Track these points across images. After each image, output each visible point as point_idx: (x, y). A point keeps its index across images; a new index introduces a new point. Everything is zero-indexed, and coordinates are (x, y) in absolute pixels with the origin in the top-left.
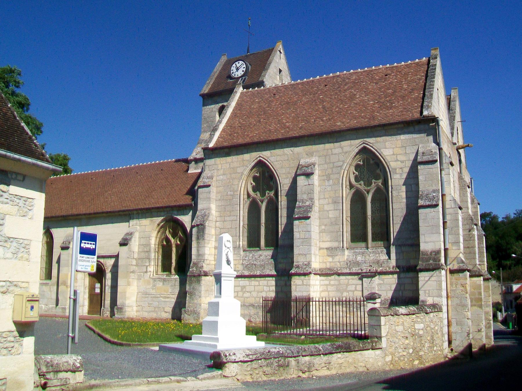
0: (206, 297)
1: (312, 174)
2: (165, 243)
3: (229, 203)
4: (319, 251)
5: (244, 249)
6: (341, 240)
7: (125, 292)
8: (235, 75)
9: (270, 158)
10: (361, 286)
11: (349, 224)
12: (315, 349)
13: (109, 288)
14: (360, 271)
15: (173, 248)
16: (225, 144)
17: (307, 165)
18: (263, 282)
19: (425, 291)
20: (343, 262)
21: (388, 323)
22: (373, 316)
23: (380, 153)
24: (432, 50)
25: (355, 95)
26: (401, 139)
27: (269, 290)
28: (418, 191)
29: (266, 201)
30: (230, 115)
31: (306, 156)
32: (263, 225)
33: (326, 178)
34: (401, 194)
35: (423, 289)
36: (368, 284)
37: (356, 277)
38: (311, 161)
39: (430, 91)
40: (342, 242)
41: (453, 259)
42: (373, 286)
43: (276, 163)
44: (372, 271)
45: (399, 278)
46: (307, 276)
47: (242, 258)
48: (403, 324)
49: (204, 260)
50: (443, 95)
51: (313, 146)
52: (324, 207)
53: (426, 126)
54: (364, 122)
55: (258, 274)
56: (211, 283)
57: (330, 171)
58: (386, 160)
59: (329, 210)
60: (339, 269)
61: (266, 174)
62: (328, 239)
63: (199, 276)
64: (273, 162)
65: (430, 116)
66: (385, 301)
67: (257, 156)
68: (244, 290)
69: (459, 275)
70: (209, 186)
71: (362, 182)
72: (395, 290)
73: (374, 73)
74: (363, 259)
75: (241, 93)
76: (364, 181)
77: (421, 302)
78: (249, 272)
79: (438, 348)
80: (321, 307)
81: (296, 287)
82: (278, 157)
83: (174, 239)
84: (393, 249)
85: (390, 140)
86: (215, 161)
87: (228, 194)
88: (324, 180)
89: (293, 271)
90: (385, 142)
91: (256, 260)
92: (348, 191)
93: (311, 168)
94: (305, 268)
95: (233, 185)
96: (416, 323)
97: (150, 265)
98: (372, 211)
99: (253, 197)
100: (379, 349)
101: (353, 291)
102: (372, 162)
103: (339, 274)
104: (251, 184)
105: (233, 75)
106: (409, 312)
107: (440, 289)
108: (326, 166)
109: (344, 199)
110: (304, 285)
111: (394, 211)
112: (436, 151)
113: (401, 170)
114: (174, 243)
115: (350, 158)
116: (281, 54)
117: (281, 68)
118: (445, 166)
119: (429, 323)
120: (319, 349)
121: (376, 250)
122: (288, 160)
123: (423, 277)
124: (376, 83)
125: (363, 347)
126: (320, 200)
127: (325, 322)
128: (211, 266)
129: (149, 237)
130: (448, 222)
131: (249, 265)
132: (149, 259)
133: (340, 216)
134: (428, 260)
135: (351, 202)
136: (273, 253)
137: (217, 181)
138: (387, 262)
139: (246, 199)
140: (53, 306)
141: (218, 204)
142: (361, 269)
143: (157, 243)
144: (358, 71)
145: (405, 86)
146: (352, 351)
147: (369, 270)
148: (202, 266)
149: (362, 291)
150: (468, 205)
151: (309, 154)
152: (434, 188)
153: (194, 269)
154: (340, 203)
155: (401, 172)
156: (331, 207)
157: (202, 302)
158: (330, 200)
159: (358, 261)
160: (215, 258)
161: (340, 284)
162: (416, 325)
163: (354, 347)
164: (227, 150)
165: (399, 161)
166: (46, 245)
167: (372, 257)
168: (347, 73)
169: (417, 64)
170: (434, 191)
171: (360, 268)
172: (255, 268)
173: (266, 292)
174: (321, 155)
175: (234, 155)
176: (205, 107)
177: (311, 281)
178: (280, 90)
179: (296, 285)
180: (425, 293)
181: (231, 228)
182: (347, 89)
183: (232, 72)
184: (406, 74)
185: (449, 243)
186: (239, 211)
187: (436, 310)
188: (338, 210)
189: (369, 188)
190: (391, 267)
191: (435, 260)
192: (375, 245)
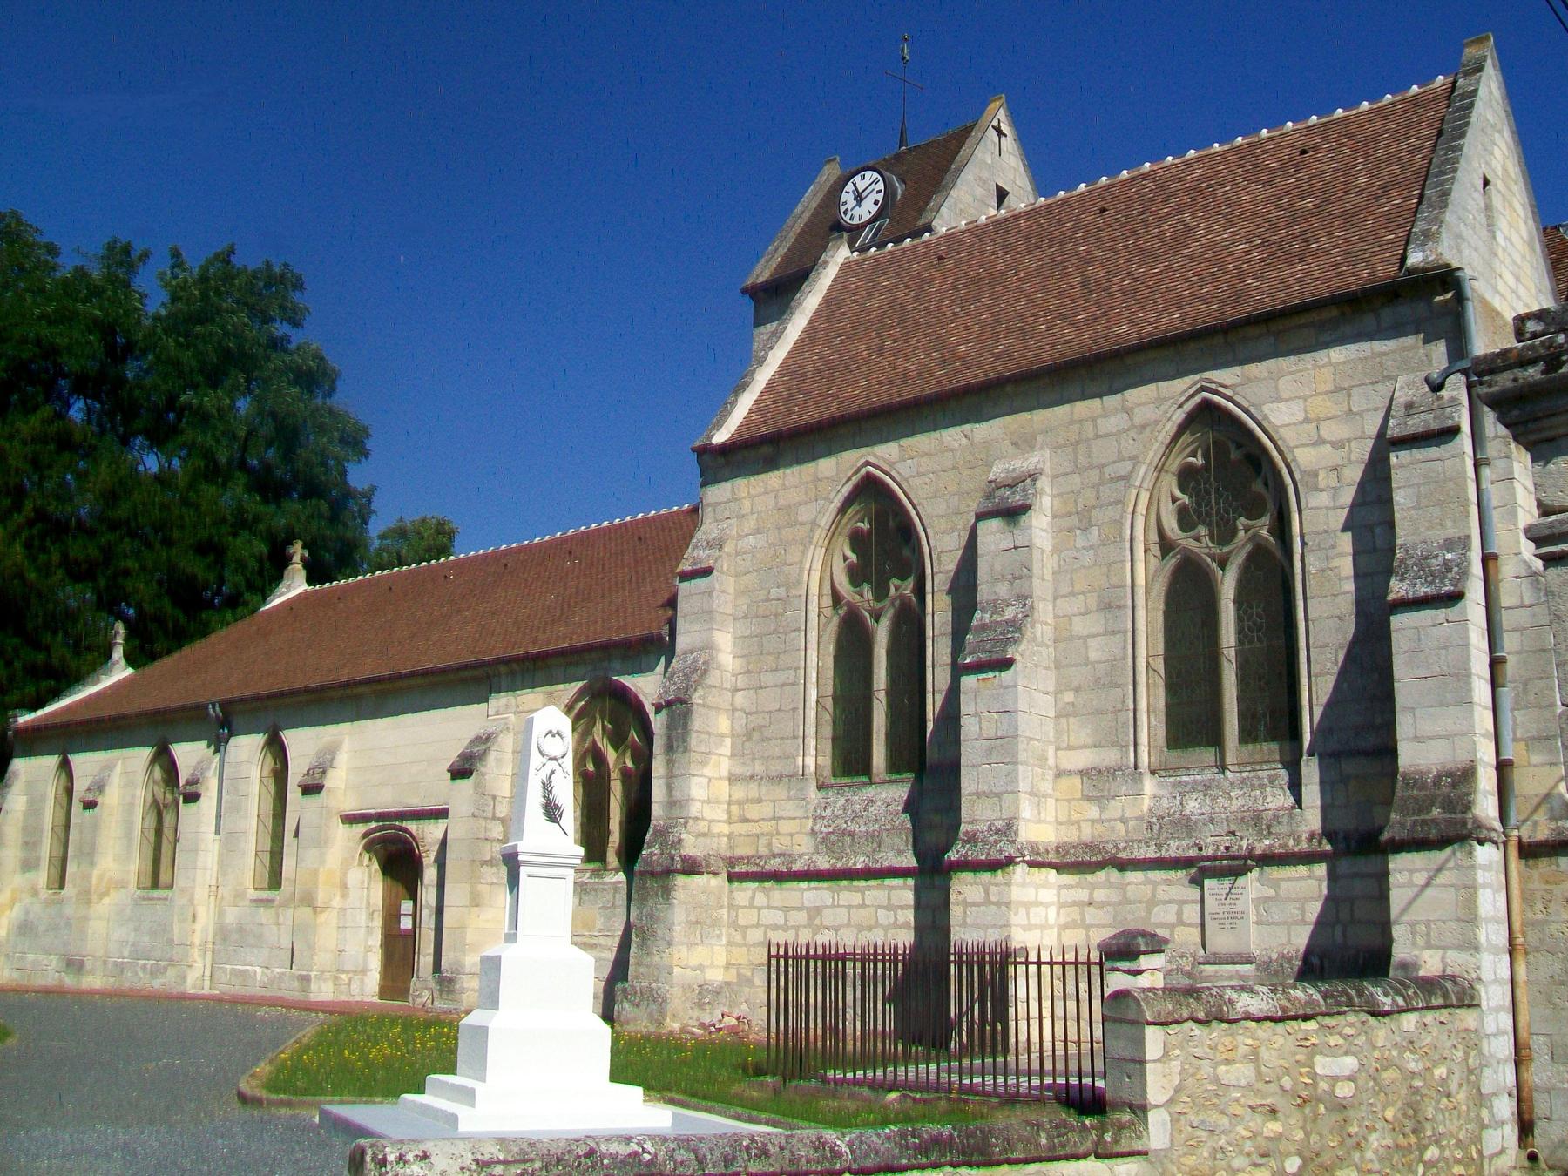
0: (690, 945)
1: (1025, 508)
2: (591, 767)
3: (773, 627)
4: (1055, 783)
6: (1128, 742)
7: (463, 928)
8: (851, 218)
9: (897, 466)
10: (1198, 907)
11: (1161, 683)
12: (816, 1149)
13: (430, 916)
14: (1192, 853)
15: (612, 783)
16: (764, 430)
17: (1010, 482)
18: (874, 892)
19: (1413, 924)
20: (1137, 819)
21: (1177, 1052)
22: (1121, 1021)
23: (1260, 418)
24: (1468, 45)
25: (1191, 229)
26: (1333, 361)
27: (895, 923)
28: (1393, 550)
29: (890, 613)
30: (797, 338)
31: (1012, 450)
32: (882, 695)
33: (1077, 524)
34: (1335, 563)
35: (1406, 918)
36: (1223, 901)
37: (1181, 874)
38: (1025, 464)
39: (1442, 183)
40: (1132, 749)
41: (1535, 801)
42: (1240, 906)
43: (918, 481)
44: (1234, 851)
45: (1332, 876)
46: (999, 872)
47: (811, 811)
48: (1254, 1056)
50: (1518, 207)
51: (1035, 412)
52: (1071, 625)
53: (1421, 308)
54: (1204, 313)
55: (859, 866)
56: (713, 898)
57: (1088, 496)
58: (1279, 443)
59: (1088, 636)
60: (1122, 845)
61: (891, 524)
63: (668, 872)
65: (1433, 269)
66: (1282, 965)
67: (858, 460)
68: (817, 922)
69: (1558, 866)
70: (707, 572)
71: (1203, 531)
72: (1321, 924)
73: (1265, 152)
75: (843, 266)
76: (1209, 525)
77: (1396, 969)
78: (833, 861)
79: (1447, 1153)
80: (1058, 984)
81: (965, 912)
82: (924, 459)
83: (616, 749)
84: (1311, 771)
85: (1295, 368)
86: (733, 487)
88: (1071, 530)
89: (953, 855)
90: (1275, 377)
91: (855, 816)
92: (1154, 562)
93: (1024, 490)
94: (996, 843)
95: (785, 564)
96: (1321, 1053)
98: (1240, 632)
99: (849, 603)
100: (1139, 1153)
102: (1235, 454)
103: (1123, 866)
104: (845, 558)
105: (847, 219)
106: (1283, 1009)
107: (1470, 917)
108: (1076, 479)
109: (1140, 592)
110: (993, 903)
111: (1311, 627)
113: (1333, 475)
114: (615, 765)
115: (1157, 445)
116: (1003, 138)
117: (1005, 184)
119: (1395, 1053)
120: (832, 1150)
121: (1253, 774)
122: (954, 468)
123: (1406, 870)
124: (1267, 183)
125: (1052, 1147)
126: (1059, 601)
127: (1076, 1038)
128: (715, 840)
130: (1512, 662)
134: (1423, 807)
135: (1167, 604)
136: (911, 794)
137: (737, 554)
138: (1291, 816)
139: (829, 612)
140: (284, 970)
142: (1196, 845)
144: (1212, 151)
145: (1361, 181)
146: (999, 1163)
147: (1227, 848)
148: (680, 841)
149: (1203, 925)
152: (1452, 532)
153: (656, 850)
154: (1125, 606)
155: (1333, 482)
157: (675, 961)
158: (1092, 601)
159: (1188, 818)
160: (729, 812)
161: (1125, 901)
162: (1318, 1059)
163: (1009, 1144)
164: (766, 450)
166: (271, 781)
167: (1238, 801)
168: (1176, 161)
169: (1415, 101)
170: (1449, 545)
172: (850, 846)
173: (886, 929)
174: (1061, 441)
175: (790, 465)
176: (762, 329)
177: (1014, 888)
178: (962, 243)
179: (966, 904)
180: (1413, 933)
182: (1167, 214)
183: (842, 209)
184: (1373, 140)
187: (1439, 1001)
188: (1119, 632)
189: (1225, 549)
190: (1305, 836)
191: (1449, 805)
192: (1251, 755)
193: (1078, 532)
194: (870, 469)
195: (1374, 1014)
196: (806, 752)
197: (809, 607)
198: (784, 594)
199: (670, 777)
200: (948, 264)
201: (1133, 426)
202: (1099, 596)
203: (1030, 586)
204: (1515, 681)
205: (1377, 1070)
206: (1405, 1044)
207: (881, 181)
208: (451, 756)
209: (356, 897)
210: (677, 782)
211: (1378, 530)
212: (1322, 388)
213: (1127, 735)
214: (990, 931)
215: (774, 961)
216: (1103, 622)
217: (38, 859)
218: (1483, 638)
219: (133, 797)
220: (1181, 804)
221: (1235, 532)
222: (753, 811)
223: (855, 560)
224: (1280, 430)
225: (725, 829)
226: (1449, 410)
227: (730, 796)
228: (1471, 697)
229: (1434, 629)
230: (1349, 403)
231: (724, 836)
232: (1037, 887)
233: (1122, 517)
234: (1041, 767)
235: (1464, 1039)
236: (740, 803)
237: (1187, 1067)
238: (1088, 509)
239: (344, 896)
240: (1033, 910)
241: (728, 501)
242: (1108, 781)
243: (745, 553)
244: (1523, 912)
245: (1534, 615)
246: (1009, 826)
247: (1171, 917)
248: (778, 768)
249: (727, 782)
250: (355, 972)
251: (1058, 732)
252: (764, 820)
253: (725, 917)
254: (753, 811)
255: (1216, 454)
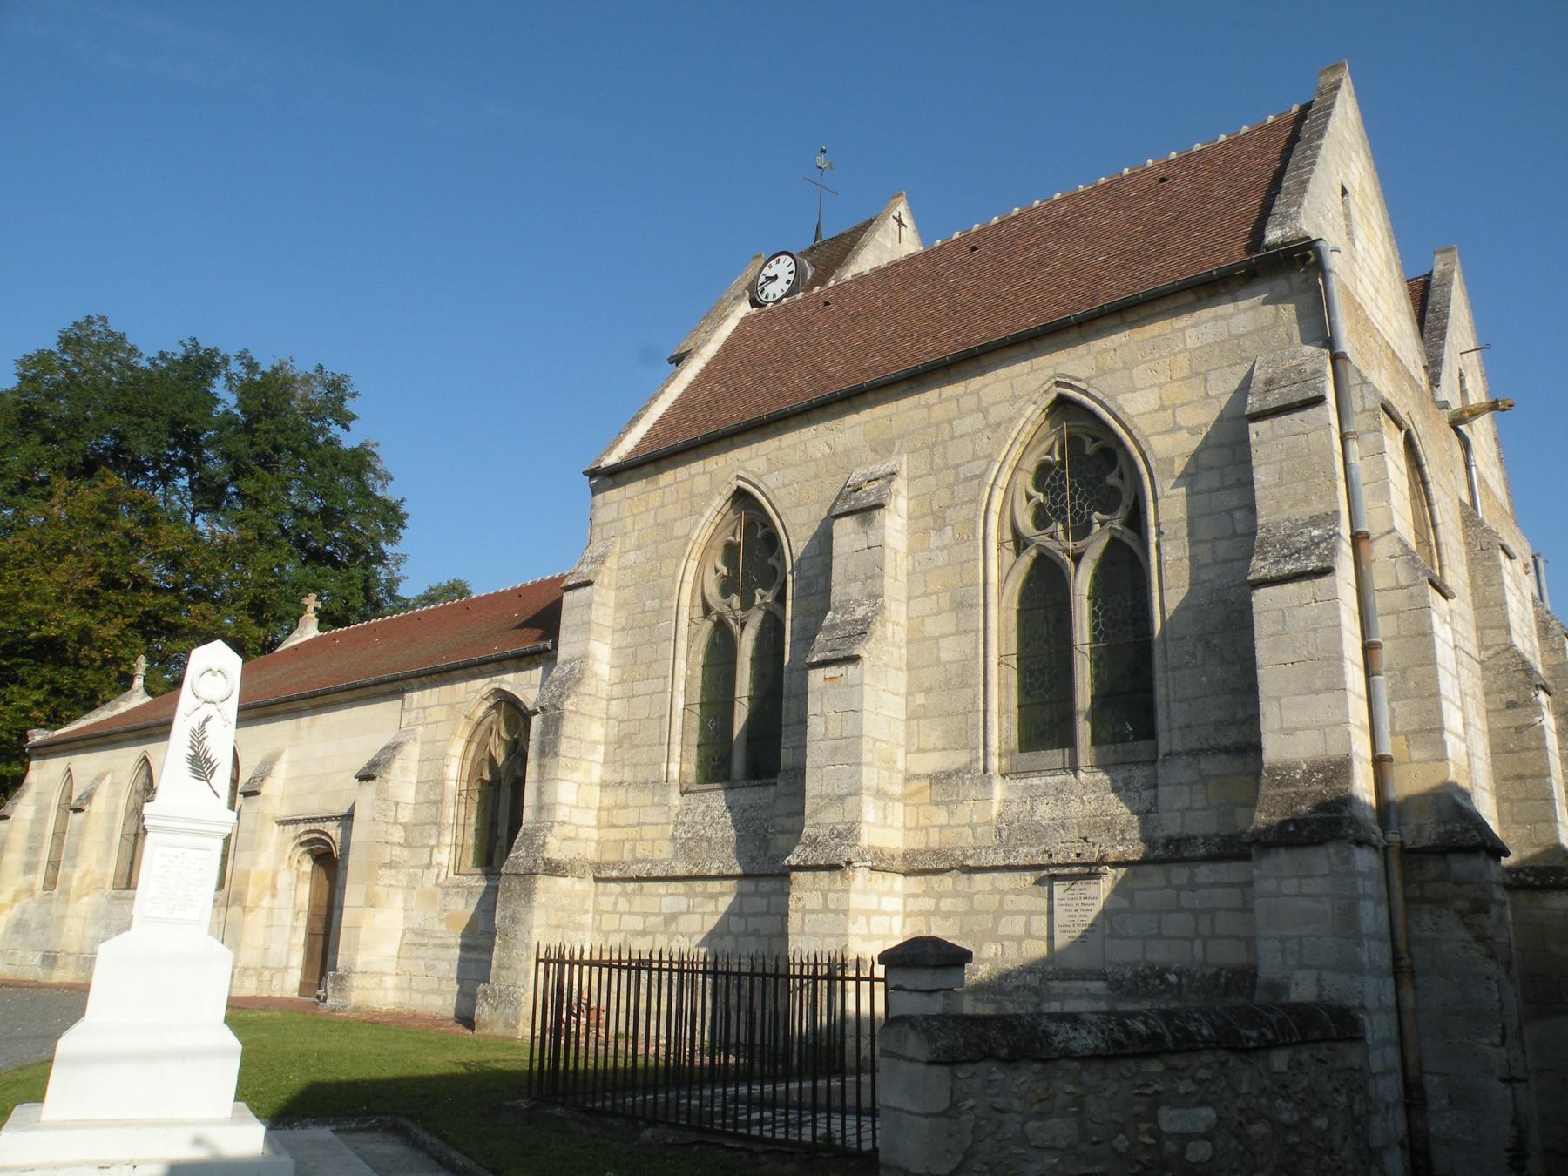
3: (646, 638)
5: (685, 786)
9: (764, 479)
10: (1044, 918)
14: (1042, 859)
20: (985, 824)
22: (899, 1057)
23: (1114, 409)
26: (1189, 347)
31: (870, 456)
33: (932, 524)
38: (882, 469)
43: (783, 492)
44: (1086, 858)
45: (740, 895)
47: (673, 817)
49: (552, 822)
59: (941, 637)
60: (971, 852)
62: (934, 737)
64: (773, 491)
68: (673, 928)
70: (589, 583)
74: (1058, 813)
76: (1064, 521)
87: (646, 609)
89: (792, 860)
92: (1009, 556)
94: (837, 846)
97: (438, 845)
101: (1019, 940)
102: (1090, 448)
104: (717, 571)
105: (763, 297)
106: (1118, 1044)
108: (932, 480)
112: (1317, 366)
118: (1357, 423)
119: (1263, 1101)
122: (817, 477)
129: (442, 758)
130: (1387, 647)
131: (691, 843)
132: (438, 824)
133: (977, 654)
141: (617, 645)
142: (1046, 852)
143: (466, 777)
150: (1505, 616)
151: (879, 449)
152: (1318, 507)
156: (947, 623)
158: (945, 601)
160: (599, 819)
161: (972, 911)
162: (1164, 1113)
165: (1180, 428)
170: (1315, 521)
171: (1043, 847)
172: (708, 852)
173: (736, 937)
179: (804, 911)
181: (648, 718)
185: (1393, 733)
186: (671, 661)
187: (1317, 1034)
188: (971, 631)
193: (933, 532)
194: (741, 483)
195: (1233, 1050)
196: (671, 758)
197: (680, 618)
198: (658, 606)
199: (541, 780)
200: (833, 307)
201: (988, 425)
202: (951, 596)
203: (882, 586)
204: (1391, 670)
205: (1240, 1124)
206: (1275, 1088)
207: (793, 264)
208: (361, 763)
209: (284, 898)
210: (548, 787)
211: (1237, 515)
212: (1178, 374)
213: (977, 737)
214: (828, 940)
215: (542, 965)
216: (955, 621)
217: (38, 862)
218: (1355, 621)
219: (117, 806)
220: (1032, 809)
221: (1089, 525)
222: (621, 817)
223: (725, 572)
224: (1135, 419)
225: (594, 834)
226: (1312, 382)
227: (601, 802)
228: (1345, 683)
229: (1302, 610)
230: (1206, 387)
231: (591, 841)
232: (881, 894)
233: (976, 515)
234: (888, 769)
235: (1347, 1080)
236: (609, 809)
237: (983, 1122)
238: (943, 509)
239: (274, 896)
240: (875, 920)
241: (614, 521)
242: (957, 785)
243: (625, 568)
244: (1407, 929)
245: (1411, 597)
246: (851, 830)
247: (1019, 930)
248: (645, 774)
249: (598, 789)
250: (277, 970)
251: (909, 735)
252: (630, 826)
253: (590, 921)
254: (621, 817)
255: (1073, 444)
